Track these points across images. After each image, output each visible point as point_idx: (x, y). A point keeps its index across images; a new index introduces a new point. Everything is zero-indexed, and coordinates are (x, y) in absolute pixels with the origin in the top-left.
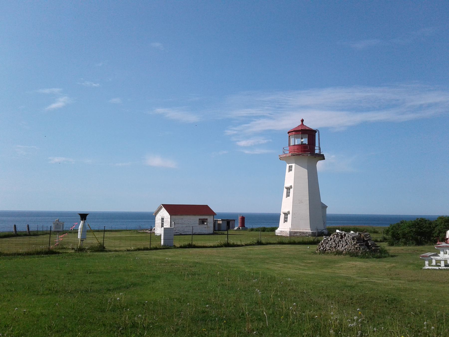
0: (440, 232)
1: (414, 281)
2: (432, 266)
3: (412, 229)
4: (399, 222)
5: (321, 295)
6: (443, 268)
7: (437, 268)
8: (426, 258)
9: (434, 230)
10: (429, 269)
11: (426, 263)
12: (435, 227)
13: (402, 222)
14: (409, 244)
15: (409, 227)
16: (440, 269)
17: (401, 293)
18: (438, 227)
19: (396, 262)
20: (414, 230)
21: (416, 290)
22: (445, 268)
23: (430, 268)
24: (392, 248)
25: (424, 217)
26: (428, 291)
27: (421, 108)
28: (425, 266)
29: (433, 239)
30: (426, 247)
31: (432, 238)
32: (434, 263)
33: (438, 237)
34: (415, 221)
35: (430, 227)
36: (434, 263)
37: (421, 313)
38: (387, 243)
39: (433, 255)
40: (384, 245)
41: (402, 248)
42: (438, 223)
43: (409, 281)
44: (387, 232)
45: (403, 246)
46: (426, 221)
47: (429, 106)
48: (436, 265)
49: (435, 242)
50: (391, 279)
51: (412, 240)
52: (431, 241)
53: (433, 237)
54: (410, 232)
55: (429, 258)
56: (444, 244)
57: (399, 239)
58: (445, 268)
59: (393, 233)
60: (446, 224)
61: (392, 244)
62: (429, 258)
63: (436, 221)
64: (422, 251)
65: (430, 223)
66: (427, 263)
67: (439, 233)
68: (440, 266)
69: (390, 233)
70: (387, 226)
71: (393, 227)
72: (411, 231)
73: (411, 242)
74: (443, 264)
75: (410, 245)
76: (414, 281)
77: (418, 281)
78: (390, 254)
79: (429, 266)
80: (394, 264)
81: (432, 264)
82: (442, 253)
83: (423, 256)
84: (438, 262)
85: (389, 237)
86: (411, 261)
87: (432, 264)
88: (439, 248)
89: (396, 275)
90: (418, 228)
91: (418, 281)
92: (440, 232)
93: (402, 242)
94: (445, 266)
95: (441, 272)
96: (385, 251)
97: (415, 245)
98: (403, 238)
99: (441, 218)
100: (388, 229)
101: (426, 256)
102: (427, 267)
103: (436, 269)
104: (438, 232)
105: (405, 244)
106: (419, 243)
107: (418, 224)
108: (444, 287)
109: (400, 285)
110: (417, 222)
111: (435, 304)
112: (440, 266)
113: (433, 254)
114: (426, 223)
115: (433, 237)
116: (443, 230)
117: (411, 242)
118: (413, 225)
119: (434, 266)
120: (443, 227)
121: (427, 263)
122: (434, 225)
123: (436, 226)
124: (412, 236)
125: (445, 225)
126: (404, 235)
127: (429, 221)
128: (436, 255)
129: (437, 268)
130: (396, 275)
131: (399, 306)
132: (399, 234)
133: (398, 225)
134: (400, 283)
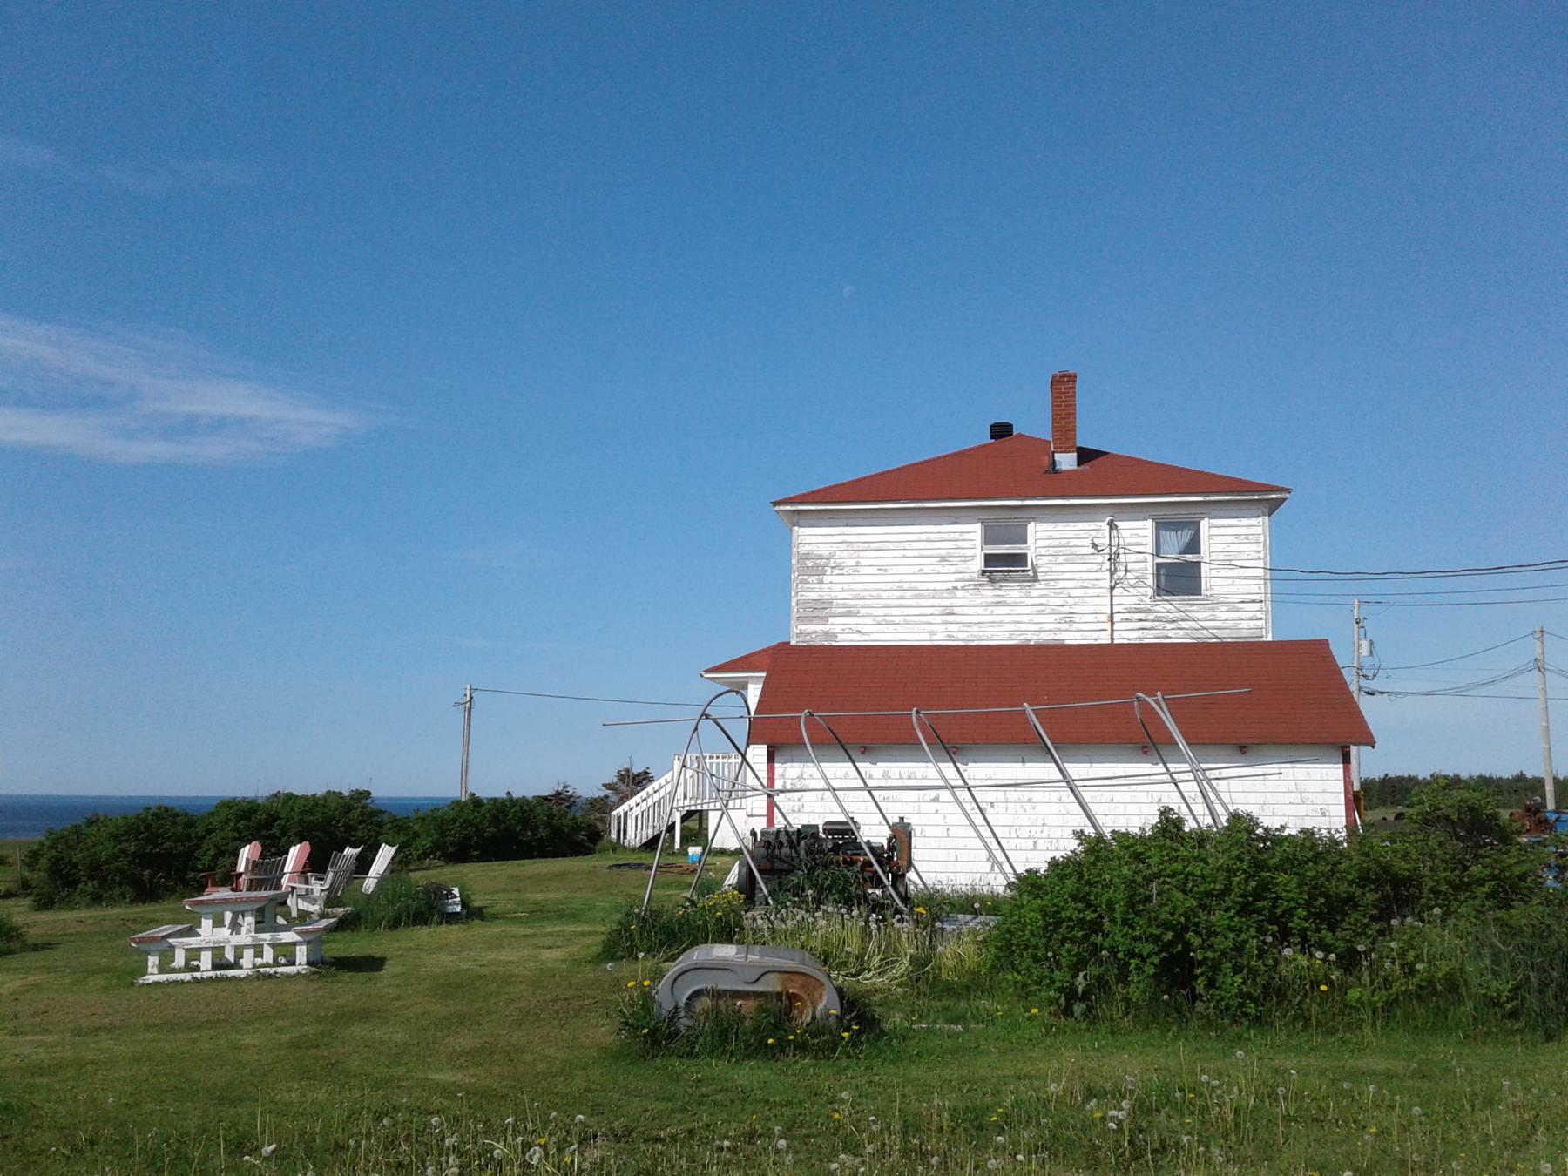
0: (220, 853)
1: (95, 1031)
2: (174, 971)
3: (125, 845)
4: (81, 821)
5: (279, 1066)
6: (206, 975)
7: (187, 977)
8: (152, 947)
9: (199, 847)
10: (157, 983)
11: (150, 964)
12: (204, 837)
13: (90, 823)
14: (110, 897)
15: (116, 837)
16: (196, 981)
17: (38, 1080)
18: (216, 837)
19: (48, 969)
20: (132, 849)
21: (92, 1063)
22: (212, 974)
23: (163, 977)
24: (45, 916)
25: (169, 804)
26: (138, 1060)
27: (189, 427)
28: (143, 971)
29: (194, 879)
30: (165, 907)
31: (191, 875)
32: (180, 959)
33: (211, 869)
34: (138, 817)
35: (188, 837)
36: (180, 959)
37: (92, 1143)
38: (28, 901)
39: (181, 934)
40: (19, 912)
41: (84, 914)
42: (215, 821)
43: (78, 1032)
44: (35, 856)
45: (88, 906)
46: (177, 815)
47: (219, 425)
48: (189, 968)
49: (201, 889)
50: (14, 1033)
51: (120, 884)
52: (186, 883)
53: (195, 869)
54: (116, 857)
55: (163, 946)
56: (224, 893)
57: (73, 884)
58: (212, 974)
59: (55, 862)
60: (240, 825)
61: (46, 904)
62: (163, 946)
63: (212, 814)
64: (151, 921)
65: (190, 824)
66: (153, 961)
67: (215, 858)
68: (197, 969)
69: (44, 862)
70: (36, 838)
71: (56, 840)
72: (123, 851)
73: (117, 890)
74: (206, 961)
75: (112, 902)
76: (95, 1031)
77: (110, 1029)
78: (30, 941)
79: (161, 971)
80: (31, 979)
81: (174, 964)
82: (207, 923)
83: (141, 941)
84: (193, 954)
85: (37, 876)
86: (104, 961)
87: (174, 964)
88: (197, 909)
89: (34, 1015)
90: (148, 840)
91: (110, 1029)
92: (220, 853)
93: (83, 893)
94: (215, 967)
95: (199, 989)
96: (12, 929)
97: (132, 902)
98: (92, 878)
99: (228, 804)
100: (35, 848)
101: (153, 940)
102: (153, 976)
103: (183, 982)
104: (212, 852)
105: (96, 899)
106: (146, 893)
107: (148, 827)
108: (195, 1041)
109: (42, 1050)
110: (144, 821)
111: (149, 1107)
112: (197, 969)
113: (179, 927)
114: (174, 824)
115: (195, 869)
116: (230, 847)
117: (117, 890)
118: (127, 833)
119: (179, 971)
120: (230, 835)
121: (153, 961)
122: (201, 830)
123: (209, 832)
124: (122, 872)
125: (236, 829)
126: (95, 870)
127: (186, 814)
128: (191, 932)
129: (187, 977)
130: (34, 1015)
131: (16, 1132)
132: (75, 866)
133: (77, 831)
134: (42, 1044)
